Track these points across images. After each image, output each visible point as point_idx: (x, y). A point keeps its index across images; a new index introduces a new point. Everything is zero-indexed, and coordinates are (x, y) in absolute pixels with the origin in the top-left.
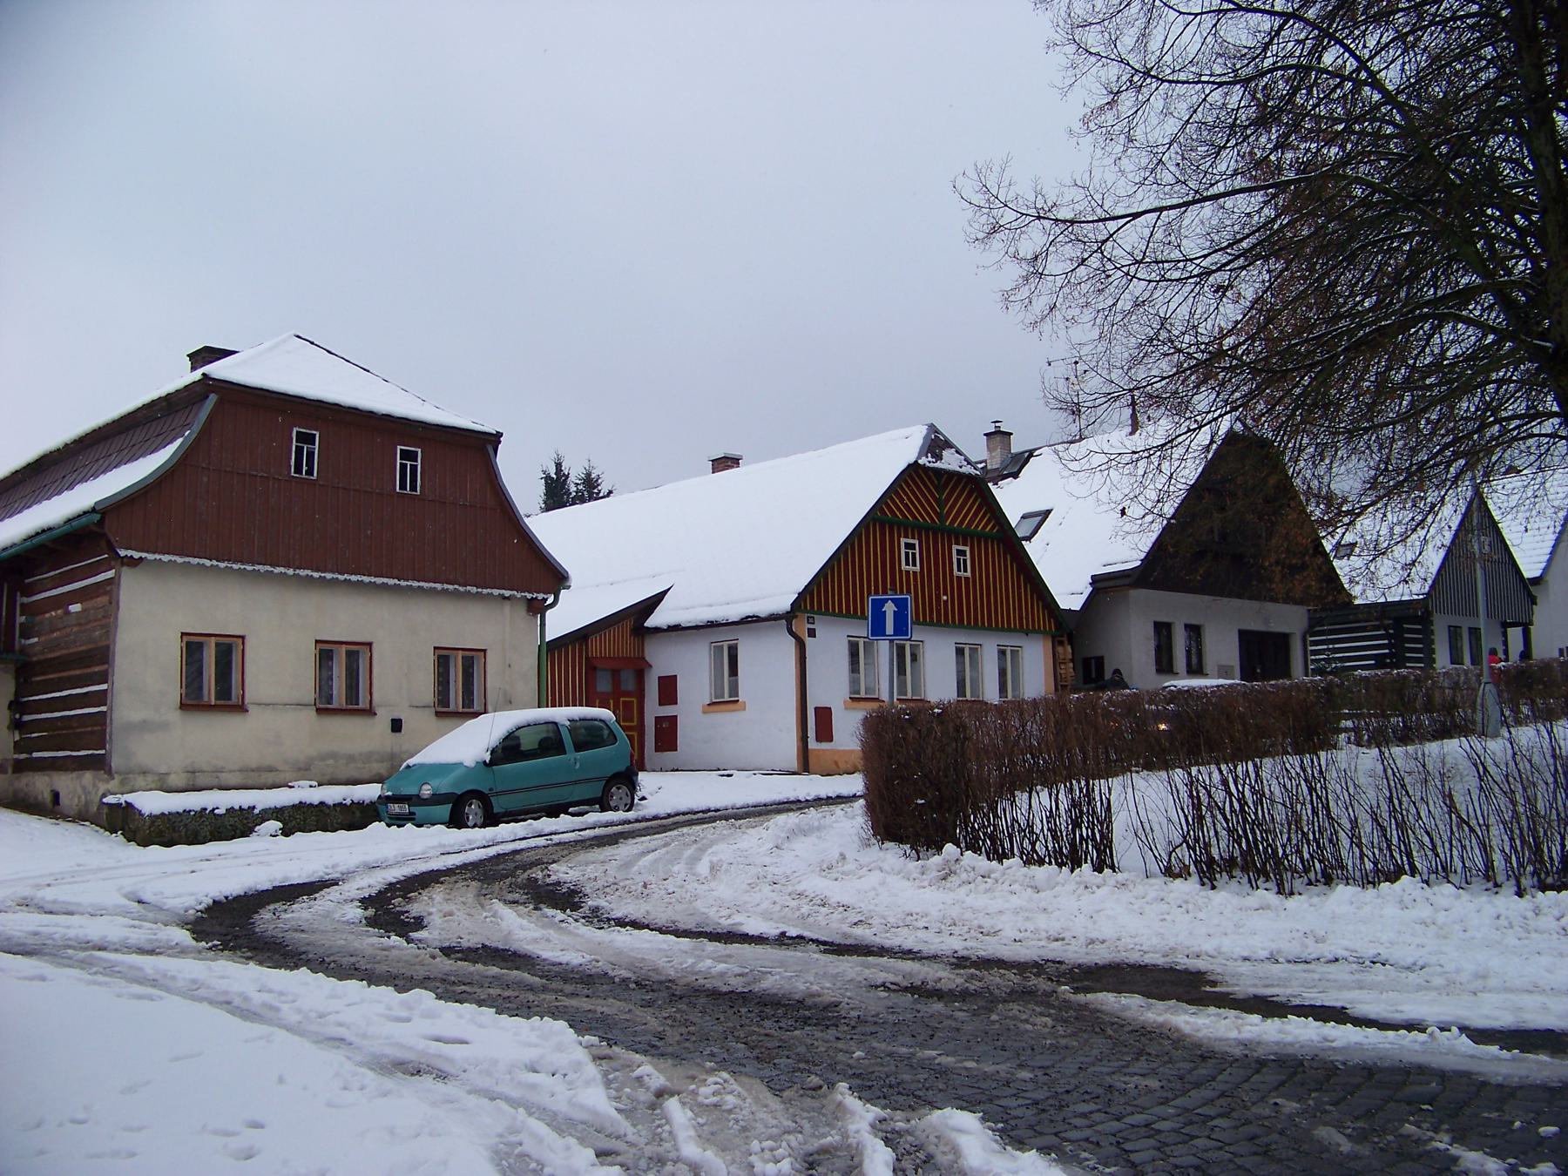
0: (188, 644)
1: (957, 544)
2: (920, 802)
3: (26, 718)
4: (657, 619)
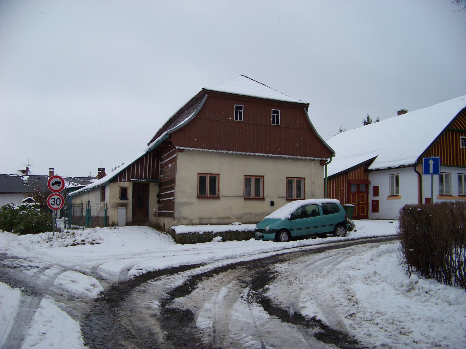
0: (200, 177)
1: (462, 136)
2: (411, 250)
3: (161, 200)
4: (373, 166)
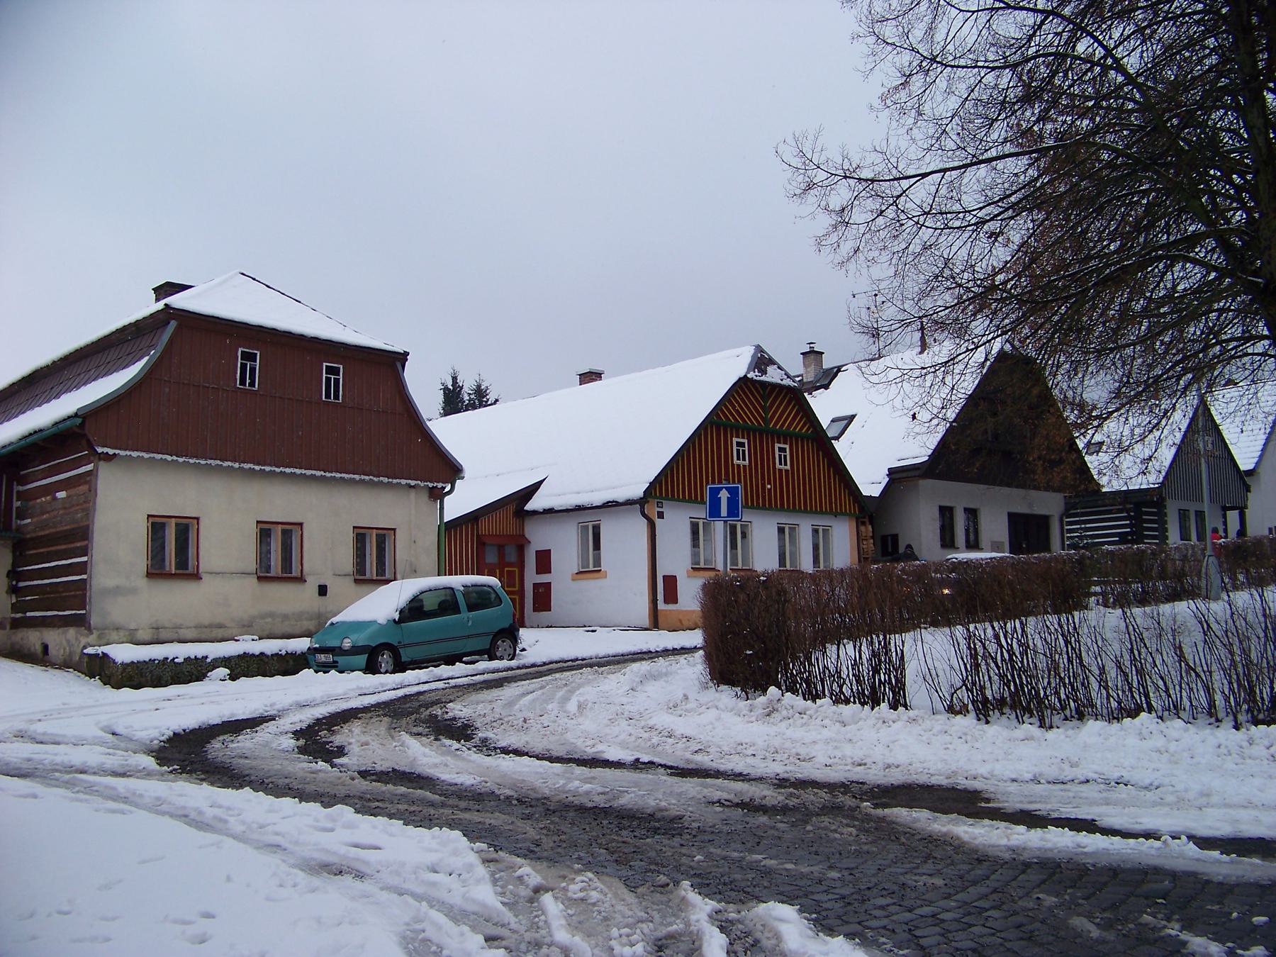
0: (153, 524)
1: (779, 442)
2: (748, 652)
3: (22, 584)
4: (535, 504)
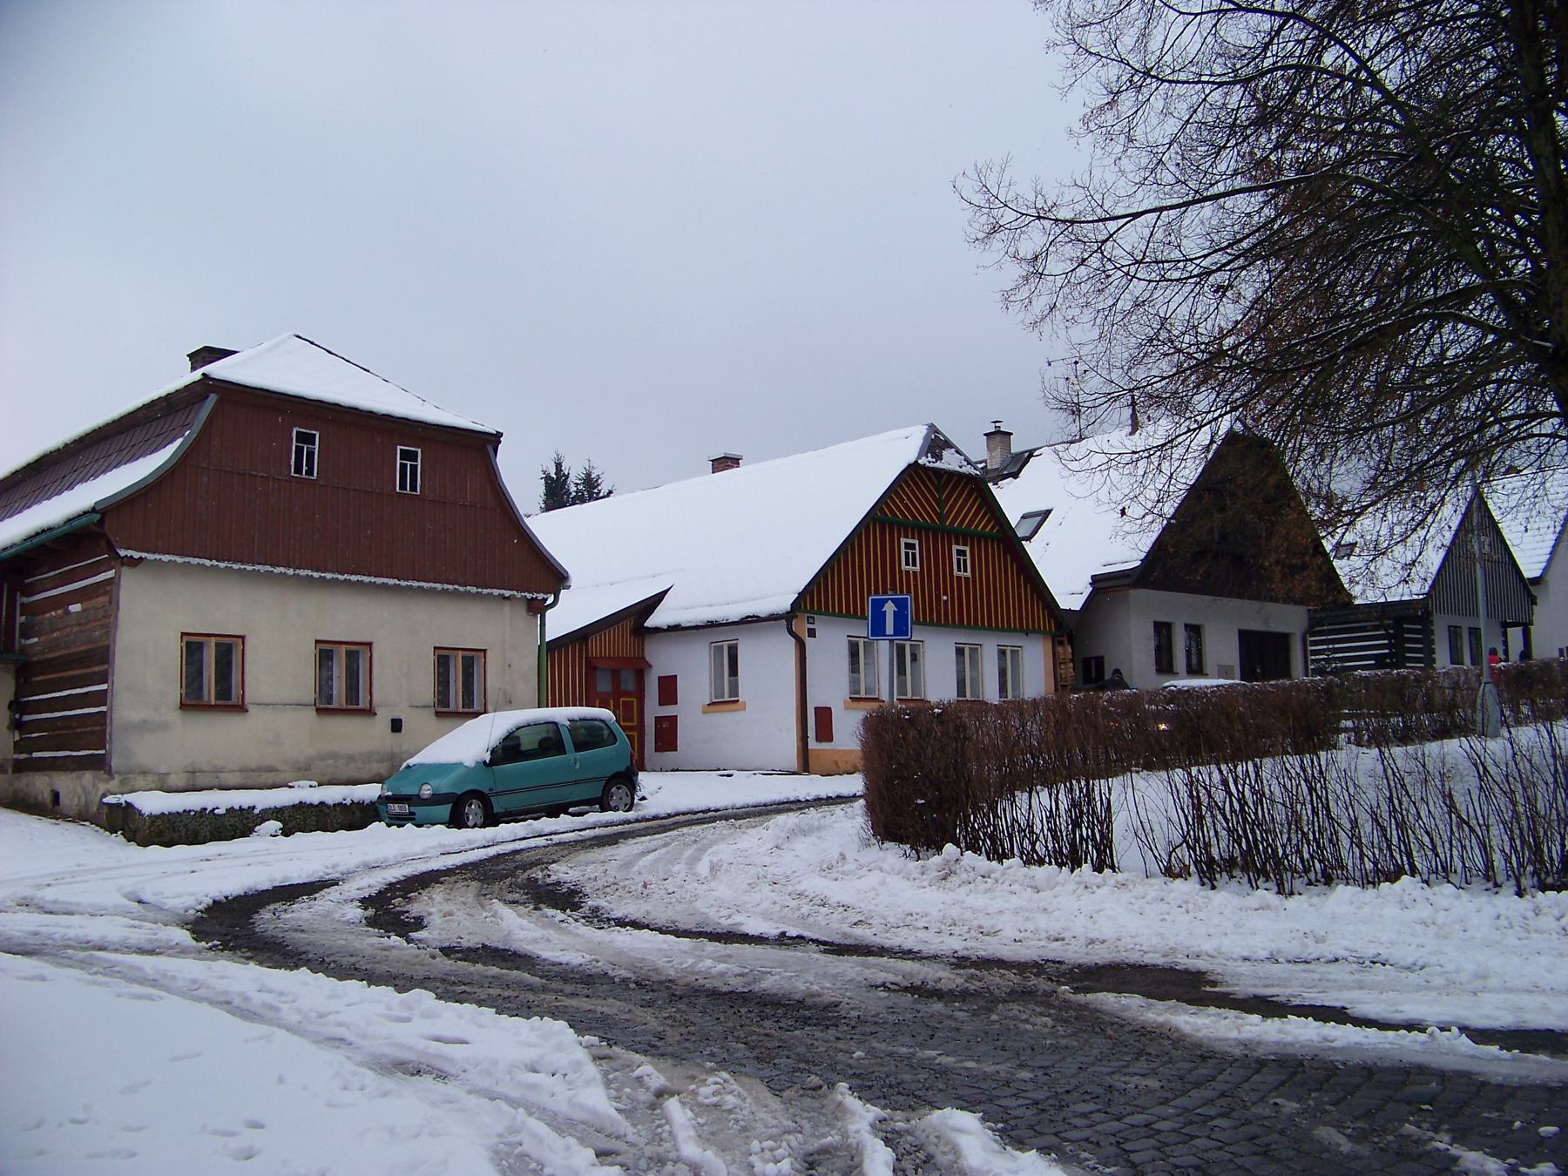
0: (188, 644)
1: (957, 544)
2: (920, 802)
3: (26, 718)
4: (657, 619)
